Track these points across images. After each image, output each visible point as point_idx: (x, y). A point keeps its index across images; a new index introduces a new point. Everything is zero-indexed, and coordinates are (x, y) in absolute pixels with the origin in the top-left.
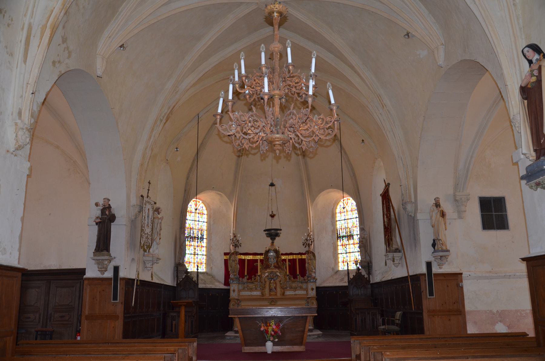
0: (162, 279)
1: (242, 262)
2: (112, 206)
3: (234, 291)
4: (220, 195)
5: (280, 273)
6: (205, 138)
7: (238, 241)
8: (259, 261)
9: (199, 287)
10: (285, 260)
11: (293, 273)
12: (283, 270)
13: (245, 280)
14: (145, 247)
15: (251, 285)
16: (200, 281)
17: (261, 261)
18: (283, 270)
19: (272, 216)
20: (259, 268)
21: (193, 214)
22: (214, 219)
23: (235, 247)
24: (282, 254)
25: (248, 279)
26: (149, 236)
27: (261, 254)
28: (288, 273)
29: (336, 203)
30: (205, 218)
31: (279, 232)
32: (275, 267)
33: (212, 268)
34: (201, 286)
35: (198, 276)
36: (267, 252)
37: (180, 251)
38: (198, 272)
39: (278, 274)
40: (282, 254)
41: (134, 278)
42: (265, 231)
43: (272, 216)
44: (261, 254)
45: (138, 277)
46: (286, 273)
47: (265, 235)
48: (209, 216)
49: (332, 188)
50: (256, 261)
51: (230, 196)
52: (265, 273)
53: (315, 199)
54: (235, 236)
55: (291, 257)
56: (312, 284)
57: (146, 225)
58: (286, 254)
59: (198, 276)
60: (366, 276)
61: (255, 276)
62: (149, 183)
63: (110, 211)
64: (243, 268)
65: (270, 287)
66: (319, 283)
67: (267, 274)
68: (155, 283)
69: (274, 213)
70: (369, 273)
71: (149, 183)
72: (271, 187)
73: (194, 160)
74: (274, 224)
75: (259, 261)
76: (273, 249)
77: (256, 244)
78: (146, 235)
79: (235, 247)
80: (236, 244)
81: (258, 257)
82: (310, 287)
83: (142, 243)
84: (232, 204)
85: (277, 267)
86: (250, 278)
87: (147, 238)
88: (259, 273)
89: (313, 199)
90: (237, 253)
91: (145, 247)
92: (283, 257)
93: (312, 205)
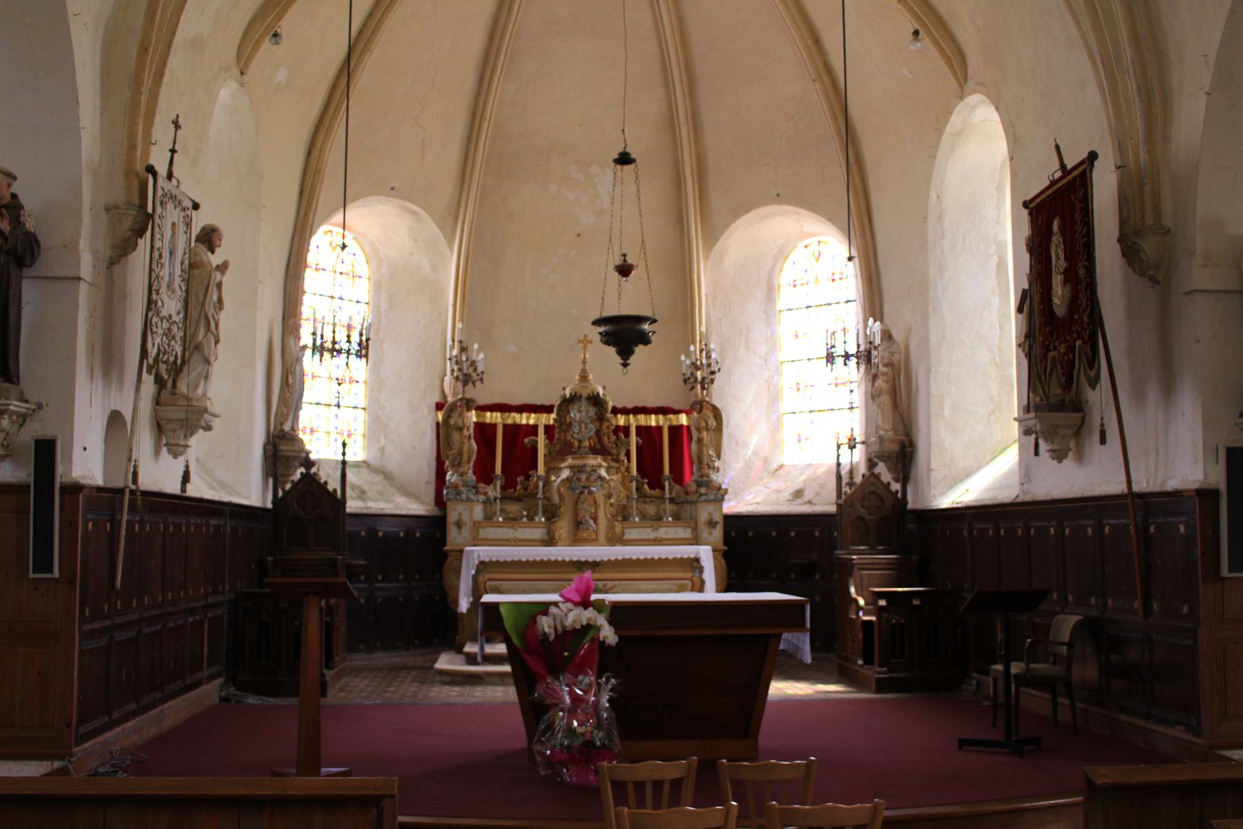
0: (224, 486)
1: (484, 432)
2: (23, 200)
3: (459, 525)
4: (414, 213)
5: (608, 469)
6: (370, 15)
7: (473, 364)
8: (541, 431)
9: (348, 510)
10: (626, 430)
11: (649, 469)
12: (617, 461)
13: (494, 491)
14: (163, 367)
15: (513, 508)
16: (349, 492)
17: (549, 429)
18: (617, 461)
19: (624, 270)
21: (327, 276)
22: (392, 286)
23: (465, 383)
24: (616, 411)
25: (503, 488)
26: (175, 330)
27: (548, 409)
28: (634, 472)
29: (782, 254)
30: (363, 290)
31: (646, 327)
32: (594, 451)
33: (382, 450)
34: (353, 506)
35: (344, 475)
36: (568, 402)
37: (286, 392)
38: (344, 463)
39: (603, 472)
40: (616, 411)
41: (120, 485)
42: (597, 322)
43: (624, 270)
45: (135, 481)
46: (628, 469)
47: (598, 337)
48: (377, 286)
49: (779, 203)
50: (533, 429)
51: (449, 220)
52: (560, 469)
54: (463, 349)
55: (642, 420)
56: (711, 508)
57: (163, 289)
58: (625, 411)
59: (344, 475)
60: (896, 486)
61: (528, 477)
62: (177, 125)
63: (16, 221)
64: (495, 452)
65: (576, 514)
66: (732, 506)
67: (565, 474)
68: (201, 500)
69: (630, 260)
70: (905, 479)
71: (177, 125)
72: (619, 167)
73: (339, 75)
74: (628, 300)
75: (541, 431)
76: (585, 395)
78: (165, 325)
79: (465, 383)
80: (465, 379)
82: (703, 517)
83: (152, 352)
84: (450, 245)
86: (509, 484)
87: (168, 333)
88: (541, 469)
89: (712, 237)
90: (469, 404)
91: (163, 367)
92: (621, 420)
93: (707, 257)
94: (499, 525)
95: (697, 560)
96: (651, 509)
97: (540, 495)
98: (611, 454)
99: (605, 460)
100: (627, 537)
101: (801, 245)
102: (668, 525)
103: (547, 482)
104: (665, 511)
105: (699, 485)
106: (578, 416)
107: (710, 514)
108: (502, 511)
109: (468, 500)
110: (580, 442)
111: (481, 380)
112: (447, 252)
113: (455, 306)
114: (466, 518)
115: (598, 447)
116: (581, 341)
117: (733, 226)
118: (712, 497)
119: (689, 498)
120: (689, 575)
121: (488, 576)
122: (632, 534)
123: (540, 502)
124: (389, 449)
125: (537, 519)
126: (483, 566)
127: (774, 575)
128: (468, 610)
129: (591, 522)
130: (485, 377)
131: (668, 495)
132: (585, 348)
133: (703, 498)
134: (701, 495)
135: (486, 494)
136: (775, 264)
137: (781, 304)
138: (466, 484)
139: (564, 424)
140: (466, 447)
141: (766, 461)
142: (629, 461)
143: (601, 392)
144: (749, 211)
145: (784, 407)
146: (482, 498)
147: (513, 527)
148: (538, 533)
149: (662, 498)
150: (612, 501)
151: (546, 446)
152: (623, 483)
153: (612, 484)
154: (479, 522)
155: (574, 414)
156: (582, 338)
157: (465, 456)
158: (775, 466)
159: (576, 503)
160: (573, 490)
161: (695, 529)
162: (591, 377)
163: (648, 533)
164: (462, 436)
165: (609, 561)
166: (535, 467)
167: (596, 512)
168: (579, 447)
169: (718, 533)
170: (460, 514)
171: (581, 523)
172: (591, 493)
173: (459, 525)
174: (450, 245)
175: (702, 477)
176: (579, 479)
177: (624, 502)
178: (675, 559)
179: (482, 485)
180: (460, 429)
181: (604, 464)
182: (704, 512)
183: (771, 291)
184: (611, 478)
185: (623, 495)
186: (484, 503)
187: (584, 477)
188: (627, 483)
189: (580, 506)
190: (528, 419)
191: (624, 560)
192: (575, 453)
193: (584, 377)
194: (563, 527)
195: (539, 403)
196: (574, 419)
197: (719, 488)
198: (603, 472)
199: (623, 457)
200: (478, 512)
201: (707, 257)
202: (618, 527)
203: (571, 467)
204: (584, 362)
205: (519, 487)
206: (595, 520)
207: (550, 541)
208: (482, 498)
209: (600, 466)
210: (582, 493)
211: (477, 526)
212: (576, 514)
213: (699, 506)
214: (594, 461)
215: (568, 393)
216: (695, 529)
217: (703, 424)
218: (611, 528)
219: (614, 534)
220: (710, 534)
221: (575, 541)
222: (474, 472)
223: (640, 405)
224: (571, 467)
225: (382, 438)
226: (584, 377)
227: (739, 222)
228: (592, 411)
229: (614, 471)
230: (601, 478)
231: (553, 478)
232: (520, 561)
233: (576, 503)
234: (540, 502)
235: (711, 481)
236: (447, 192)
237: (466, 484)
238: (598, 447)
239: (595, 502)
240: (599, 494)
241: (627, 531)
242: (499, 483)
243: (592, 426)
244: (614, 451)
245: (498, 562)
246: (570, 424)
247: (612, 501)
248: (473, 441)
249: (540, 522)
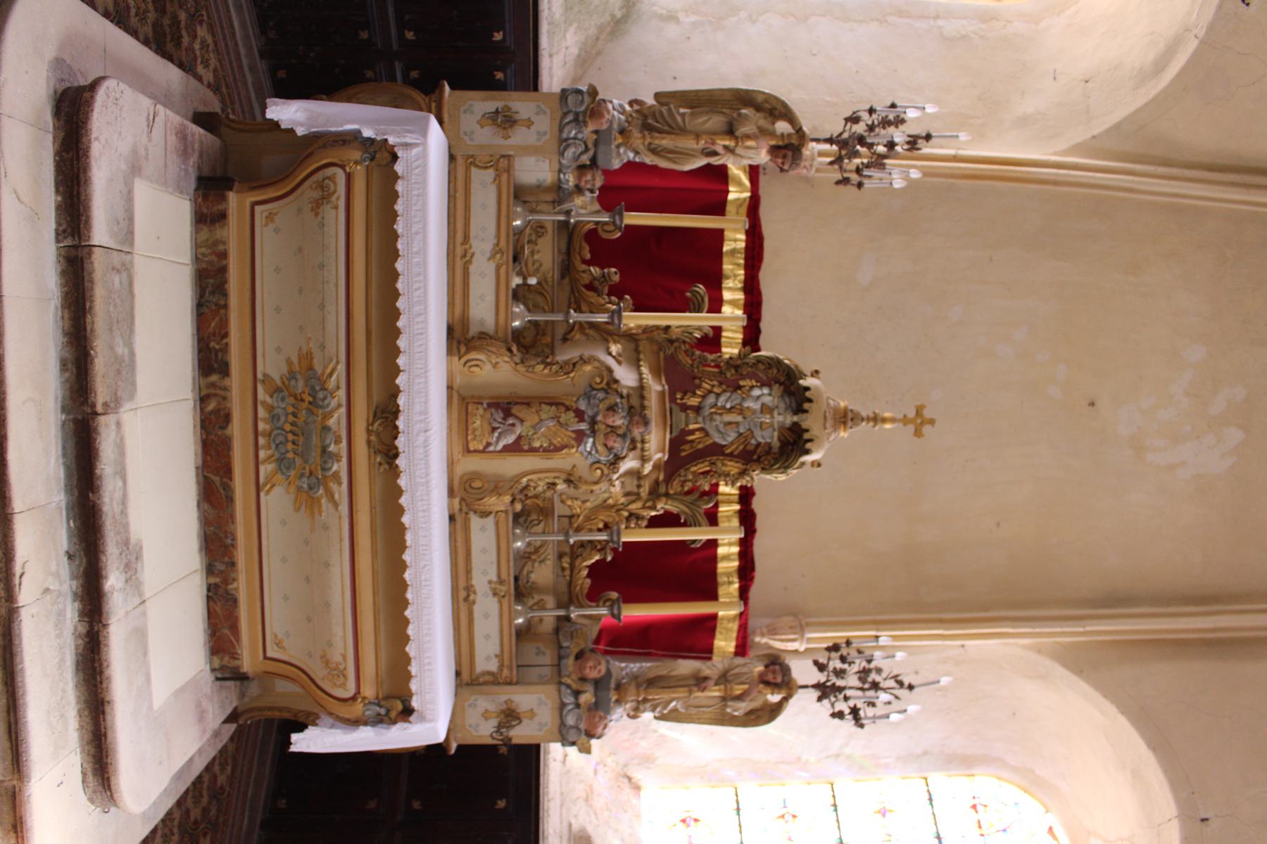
4: (1160, 66)
5: (636, 474)
12: (655, 494)
13: (586, 210)
15: (546, 254)
17: (712, 340)
20: (676, 320)
25: (592, 236)
27: (752, 336)
28: (627, 538)
29: (1034, 784)
32: (676, 444)
33: (671, 18)
36: (788, 383)
39: (629, 464)
44: (752, 336)
51: (1141, 147)
52: (636, 364)
53: (1079, 671)
56: (546, 715)
61: (616, 291)
65: (527, 402)
66: (560, 763)
67: (626, 377)
76: (808, 421)
77: (814, 289)
79: (846, 145)
81: (732, 314)
82: (524, 699)
85: (681, 455)
86: (601, 248)
88: (634, 320)
89: (1082, 662)
94: (503, 217)
95: (407, 713)
96: (543, 573)
97: (574, 316)
98: (668, 480)
99: (656, 467)
100: (475, 522)
101: (1052, 819)
102: (505, 617)
103: (605, 334)
104: (541, 606)
105: (600, 684)
106: (756, 406)
107: (532, 714)
108: (539, 229)
109: (564, 143)
110: (698, 409)
111: (846, 181)
112: (1063, 145)
113: (955, 159)
114: (520, 136)
115: (686, 451)
116: (919, 411)
117: (1112, 710)
118: (570, 720)
119: (570, 661)
120: (369, 691)
121: (359, 171)
122: (483, 534)
123: (559, 317)
124: (672, 30)
125: (519, 309)
126: (382, 158)
127: (416, 805)
128: (276, 125)
129: (510, 439)
130: (850, 190)
131: (574, 614)
132: (905, 421)
133: (569, 699)
134: (577, 693)
135: (579, 190)
136: (1015, 769)
137: (939, 780)
138: (601, 138)
139: (734, 376)
140: (688, 143)
141: (647, 760)
142: (655, 523)
143: (807, 458)
144: (1154, 746)
145: (750, 791)
146: (570, 179)
147: (497, 250)
148: (483, 311)
149: (568, 599)
150: (561, 487)
151: (687, 330)
152: (604, 506)
153: (603, 486)
154: (508, 170)
155: (761, 396)
156: (927, 414)
157: (666, 142)
158: (637, 775)
159: (554, 403)
160: (587, 397)
161: (495, 680)
162: (843, 434)
163: (485, 569)
164: (714, 133)
165: (399, 492)
166: (638, 308)
167: (533, 450)
168: (685, 408)
169: (482, 731)
170: (529, 123)
171: (507, 414)
172: (580, 437)
173: (505, 121)
174: (1077, 149)
175: (619, 687)
176: (612, 409)
177: (560, 509)
178: (407, 660)
179: (599, 182)
180: (730, 131)
181: (648, 468)
182: (536, 706)
183: (964, 762)
184: (612, 482)
185: (577, 507)
186: (558, 187)
187: (619, 421)
188: (603, 517)
189: (547, 411)
190: (733, 303)
191: (402, 529)
192: (673, 399)
193: (845, 418)
194: (497, 371)
195: (764, 325)
196: (748, 396)
197: (590, 735)
198: (629, 464)
199: (662, 506)
200: (536, 170)
201: (1039, 650)
202: (499, 503)
203: (641, 388)
204: (876, 419)
205: (595, 271)
206: (515, 448)
207: (461, 338)
208: (570, 179)
209: (644, 460)
210: (580, 415)
211: (501, 164)
212: (527, 402)
213: (551, 689)
214: (656, 443)
215: (808, 382)
216: (495, 680)
217: (738, 690)
218: (496, 486)
219: (482, 493)
220: (486, 715)
221: (462, 401)
222: (630, 165)
223: (759, 523)
224: (641, 388)
225: (693, 18)
226: (845, 418)
227: (1123, 721)
228: (769, 437)
229: (631, 485)
230: (618, 459)
231: (615, 348)
232: (396, 255)
233: (554, 403)
234: (559, 317)
235: (608, 711)
236: (1206, 134)
237: (601, 138)
238: (686, 451)
239: (558, 449)
240: (577, 458)
241: (490, 521)
242: (605, 218)
243: (732, 436)
244: (675, 487)
245: (395, 196)
246: (740, 387)
247: (561, 487)
248: (701, 162)
249: (511, 316)
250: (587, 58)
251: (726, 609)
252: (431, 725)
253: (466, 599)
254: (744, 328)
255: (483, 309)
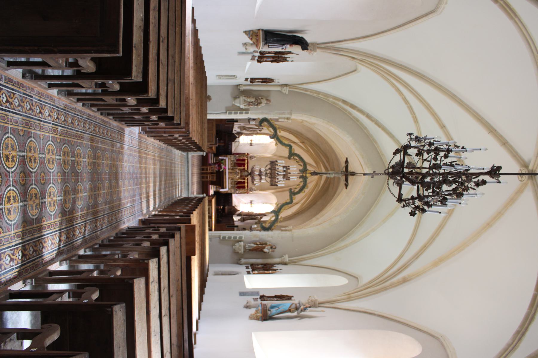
13: (235, 161)
17: (244, 169)
85: (241, 176)
86: (236, 164)
194: (230, 171)
200: (232, 159)
207: (229, 169)
221: (229, 173)
250: (235, 149)
251: (246, 185)
252: (227, 189)
253: (350, 297)
254: (290, 45)
255: (230, 167)
